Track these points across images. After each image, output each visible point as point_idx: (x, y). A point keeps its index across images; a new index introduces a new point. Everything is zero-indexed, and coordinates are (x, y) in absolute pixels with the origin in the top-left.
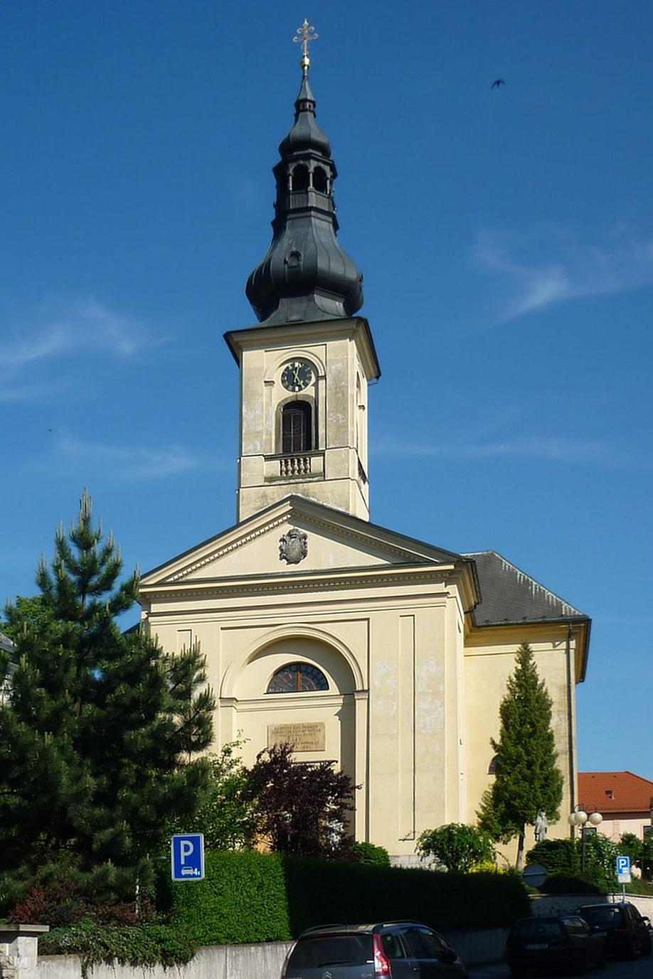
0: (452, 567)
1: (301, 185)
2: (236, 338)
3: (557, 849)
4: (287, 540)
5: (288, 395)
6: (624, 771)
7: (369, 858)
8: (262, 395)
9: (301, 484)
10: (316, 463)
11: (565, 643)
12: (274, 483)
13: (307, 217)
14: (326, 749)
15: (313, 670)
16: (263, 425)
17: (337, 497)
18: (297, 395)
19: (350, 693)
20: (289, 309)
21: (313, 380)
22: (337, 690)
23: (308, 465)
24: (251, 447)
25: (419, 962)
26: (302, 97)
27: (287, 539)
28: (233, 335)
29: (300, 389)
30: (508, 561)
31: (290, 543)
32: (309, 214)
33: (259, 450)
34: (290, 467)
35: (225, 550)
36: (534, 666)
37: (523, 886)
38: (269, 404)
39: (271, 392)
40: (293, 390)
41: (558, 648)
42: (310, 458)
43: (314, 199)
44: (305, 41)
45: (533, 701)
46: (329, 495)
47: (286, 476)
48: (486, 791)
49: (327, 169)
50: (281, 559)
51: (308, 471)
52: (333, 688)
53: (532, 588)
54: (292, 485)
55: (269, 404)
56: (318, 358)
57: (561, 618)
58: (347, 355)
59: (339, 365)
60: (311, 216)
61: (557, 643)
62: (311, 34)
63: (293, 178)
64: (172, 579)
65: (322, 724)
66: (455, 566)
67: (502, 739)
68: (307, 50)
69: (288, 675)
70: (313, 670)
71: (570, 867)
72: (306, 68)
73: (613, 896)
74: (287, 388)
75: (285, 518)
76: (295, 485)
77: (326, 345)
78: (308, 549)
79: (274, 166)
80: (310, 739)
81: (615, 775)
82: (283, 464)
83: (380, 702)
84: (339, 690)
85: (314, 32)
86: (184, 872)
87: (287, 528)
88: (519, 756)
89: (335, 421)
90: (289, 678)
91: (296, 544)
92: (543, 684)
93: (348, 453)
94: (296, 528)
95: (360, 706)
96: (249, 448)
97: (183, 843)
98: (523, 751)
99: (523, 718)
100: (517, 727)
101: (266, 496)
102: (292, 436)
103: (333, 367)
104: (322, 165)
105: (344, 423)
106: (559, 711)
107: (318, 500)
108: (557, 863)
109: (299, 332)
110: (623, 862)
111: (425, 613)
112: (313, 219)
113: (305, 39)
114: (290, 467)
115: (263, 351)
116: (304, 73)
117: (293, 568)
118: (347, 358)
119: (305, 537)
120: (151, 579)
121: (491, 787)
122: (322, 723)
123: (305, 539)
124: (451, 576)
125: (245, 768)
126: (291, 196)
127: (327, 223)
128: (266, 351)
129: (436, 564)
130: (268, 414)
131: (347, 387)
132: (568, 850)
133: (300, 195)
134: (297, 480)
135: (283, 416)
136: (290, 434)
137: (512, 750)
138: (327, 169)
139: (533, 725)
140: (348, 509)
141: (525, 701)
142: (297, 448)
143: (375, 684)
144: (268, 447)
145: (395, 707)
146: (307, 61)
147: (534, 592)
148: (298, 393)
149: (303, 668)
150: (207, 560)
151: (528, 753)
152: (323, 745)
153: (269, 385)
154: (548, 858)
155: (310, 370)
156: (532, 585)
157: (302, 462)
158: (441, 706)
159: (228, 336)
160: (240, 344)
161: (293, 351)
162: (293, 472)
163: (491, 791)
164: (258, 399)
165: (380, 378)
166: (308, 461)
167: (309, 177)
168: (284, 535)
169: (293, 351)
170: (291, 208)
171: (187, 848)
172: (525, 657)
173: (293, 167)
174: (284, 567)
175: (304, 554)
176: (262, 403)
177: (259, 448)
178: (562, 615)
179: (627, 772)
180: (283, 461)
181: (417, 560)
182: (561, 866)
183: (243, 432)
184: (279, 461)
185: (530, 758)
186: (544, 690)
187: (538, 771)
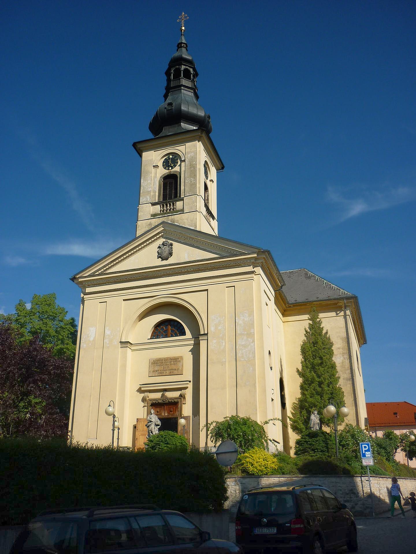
0: (256, 255)
1: (177, 76)
2: (139, 146)
3: (317, 437)
4: (161, 247)
5: (165, 172)
6: (403, 401)
7: (168, 443)
8: (151, 173)
9: (170, 216)
10: (179, 205)
11: (343, 312)
12: (156, 217)
13: (180, 89)
14: (184, 374)
16: (151, 188)
17: (190, 222)
18: (170, 172)
19: (197, 336)
20: (167, 131)
21: (179, 163)
22: (191, 336)
23: (175, 206)
24: (144, 199)
26: (180, 41)
27: (162, 246)
28: (137, 145)
30: (311, 272)
31: (163, 249)
32: (180, 88)
33: (149, 200)
34: (165, 208)
35: (127, 255)
36: (320, 322)
38: (155, 177)
39: (157, 171)
40: (169, 169)
41: (339, 315)
42: (176, 203)
43: (184, 82)
44: (183, 21)
45: (320, 343)
46: (186, 221)
47: (163, 213)
48: (295, 403)
49: (191, 70)
50: (158, 258)
51: (175, 209)
52: (189, 334)
54: (165, 217)
55: (155, 177)
56: (182, 153)
57: (339, 297)
58: (197, 148)
59: (192, 154)
60: (181, 89)
61: (338, 312)
62: (185, 17)
63: (173, 74)
64: (98, 273)
65: (181, 357)
66: (257, 255)
67: (303, 369)
68: (184, 24)
69: (163, 328)
71: (328, 452)
72: (183, 31)
73: (361, 477)
74: (165, 168)
75: (160, 235)
77: (185, 145)
78: (173, 251)
79: (165, 72)
80: (174, 367)
81: (398, 404)
82: (162, 207)
83: (214, 341)
84: (192, 336)
85: (187, 16)
87: (161, 241)
88: (313, 378)
89: (189, 182)
90: (164, 329)
91: (166, 249)
92: (327, 333)
93: (197, 197)
94: (167, 240)
95: (203, 344)
96: (143, 200)
98: (315, 375)
99: (314, 353)
100: (311, 360)
101: (151, 224)
102: (168, 193)
103: (189, 155)
105: (195, 182)
106: (343, 353)
108: (317, 449)
109: (170, 140)
111: (241, 285)
112: (182, 90)
113: (183, 20)
115: (153, 151)
116: (182, 33)
117: (165, 262)
118: (197, 150)
119: (171, 245)
120: (85, 273)
121: (297, 400)
122: (181, 356)
123: (172, 246)
126: (172, 82)
127: (191, 93)
128: (154, 151)
129: (245, 254)
130: (154, 182)
131: (196, 164)
132: (326, 438)
133: (177, 81)
134: (168, 215)
135: (163, 184)
136: (167, 192)
137: (308, 374)
138: (191, 70)
139: (321, 358)
140: (196, 227)
141: (315, 343)
142: (170, 198)
143: (212, 329)
144: (154, 199)
145: (224, 344)
146: (183, 28)
148: (171, 171)
149: (172, 323)
150: (117, 261)
151: (319, 377)
152: (182, 370)
153: (156, 168)
154: (310, 445)
155: (177, 159)
157: (172, 205)
158: (252, 343)
159: (134, 145)
161: (170, 149)
162: (166, 211)
163: (297, 403)
166: (175, 204)
167: (181, 73)
168: (160, 245)
169: (170, 149)
170: (172, 86)
173: (173, 69)
174: (159, 262)
175: (171, 254)
176: (151, 176)
177: (149, 199)
179: (405, 402)
182: (321, 452)
183: (141, 192)
184: (159, 205)
185: (320, 379)
186: (328, 335)
187: (326, 388)
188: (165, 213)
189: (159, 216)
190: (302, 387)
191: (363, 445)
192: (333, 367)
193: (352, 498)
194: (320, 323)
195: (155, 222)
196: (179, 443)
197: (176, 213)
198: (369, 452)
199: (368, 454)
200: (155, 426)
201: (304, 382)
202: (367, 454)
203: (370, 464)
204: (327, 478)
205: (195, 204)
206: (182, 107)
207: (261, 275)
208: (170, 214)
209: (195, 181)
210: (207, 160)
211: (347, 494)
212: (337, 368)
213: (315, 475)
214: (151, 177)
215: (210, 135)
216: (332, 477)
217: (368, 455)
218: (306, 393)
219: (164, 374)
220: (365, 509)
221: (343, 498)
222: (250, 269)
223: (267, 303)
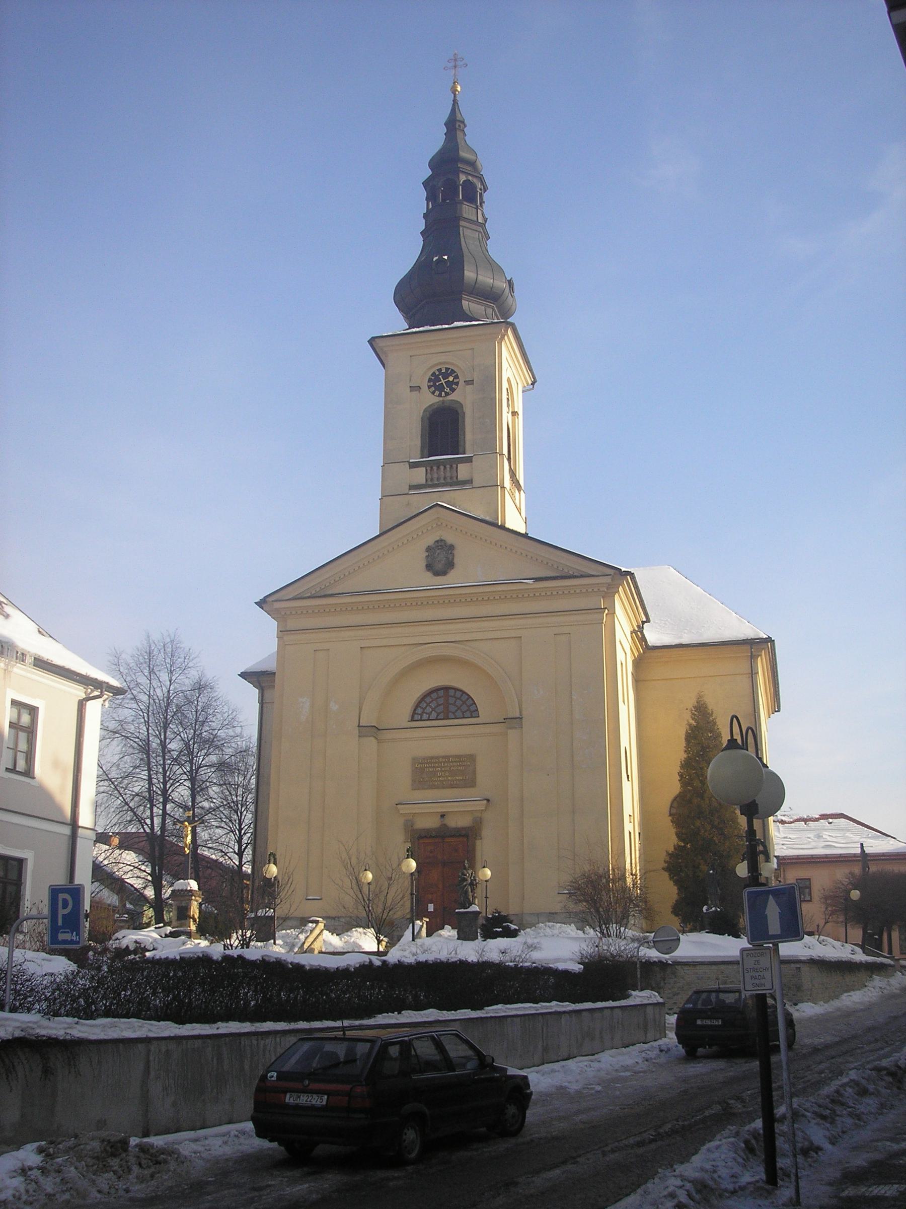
15: (462, 695)
18: (443, 400)
25: (454, 1071)
29: (447, 394)
37: (509, 965)
40: (440, 395)
70: (462, 695)
82: (429, 471)
86: (61, 937)
97: (62, 896)
104: (470, 178)
114: (448, 474)
117: (440, 580)
124: (609, 591)
138: (475, 181)
148: (445, 399)
160: (385, 349)
162: (445, 478)
165: (536, 384)
171: (65, 904)
174: (429, 579)
175: (450, 565)
206: (465, 272)
207: (530, 390)
214: (799, 881)
219: (164, 1049)
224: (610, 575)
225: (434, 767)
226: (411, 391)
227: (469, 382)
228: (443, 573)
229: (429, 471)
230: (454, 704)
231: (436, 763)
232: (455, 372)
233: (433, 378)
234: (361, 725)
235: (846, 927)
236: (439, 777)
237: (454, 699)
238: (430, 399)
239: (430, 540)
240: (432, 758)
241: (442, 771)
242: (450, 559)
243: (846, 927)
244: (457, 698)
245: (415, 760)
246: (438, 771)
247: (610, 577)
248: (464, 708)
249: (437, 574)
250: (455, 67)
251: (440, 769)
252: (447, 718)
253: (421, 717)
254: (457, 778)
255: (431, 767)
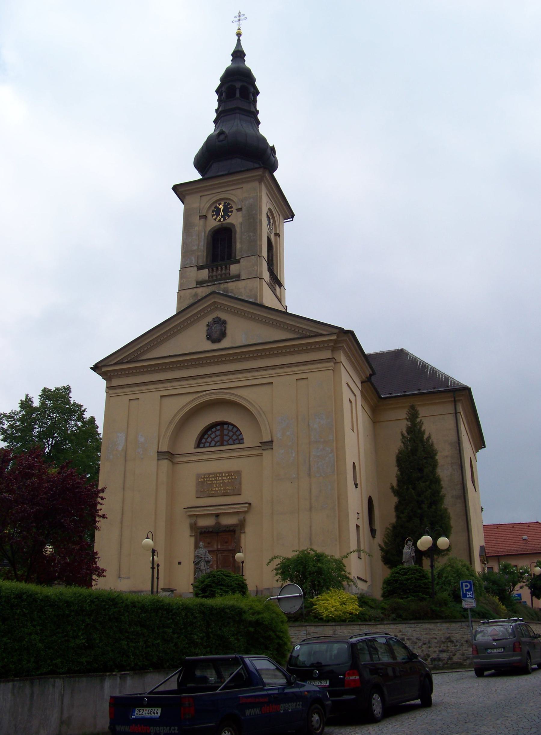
0: (334, 337)
10: (234, 269)
18: (222, 224)
36: (421, 423)
47: (211, 280)
48: (388, 528)
53: (427, 370)
76: (218, 285)
91: (217, 328)
92: (429, 437)
93: (257, 259)
96: (187, 262)
103: (247, 202)
106: (452, 463)
107: (234, 295)
110: (466, 586)
121: (391, 525)
125: (102, 500)
140: (256, 299)
147: (429, 373)
152: (240, 489)
156: (428, 368)
164: (195, 228)
172: (413, 416)
174: (210, 346)
175: (223, 334)
177: (193, 261)
178: (448, 386)
179: (537, 522)
180: (210, 269)
181: (308, 334)
186: (430, 441)
188: (216, 280)
189: (207, 284)
190: (397, 508)
191: (464, 584)
192: (437, 481)
193: (449, 647)
194: (421, 423)
195: (202, 291)
196: (236, 584)
197: (229, 280)
198: (471, 592)
199: (470, 594)
200: (205, 563)
201: (399, 502)
202: (470, 594)
203: (472, 606)
204: (420, 625)
205: (256, 267)
208: (222, 281)
209: (255, 237)
210: (271, 208)
211: (444, 643)
212: (442, 483)
213: (406, 621)
215: (275, 174)
216: (425, 623)
217: (470, 595)
218: (402, 515)
220: (465, 660)
221: (438, 648)
222: (327, 354)
223: (351, 400)
224: (335, 333)
225: (212, 481)
226: (200, 219)
227: (239, 210)
228: (217, 340)
229: (210, 271)
230: (227, 435)
231: (213, 477)
232: (230, 204)
233: (215, 209)
234: (159, 451)
235: (383, 421)
236: (215, 488)
237: (227, 431)
238: (213, 223)
239: (209, 319)
240: (210, 474)
241: (216, 483)
242: (223, 330)
243: (383, 421)
244: (229, 431)
245: (198, 476)
246: (215, 483)
247: (336, 334)
248: (234, 437)
249: (214, 341)
250: (239, 20)
251: (215, 482)
252: (222, 445)
253: (204, 445)
254: (228, 488)
255: (210, 481)
